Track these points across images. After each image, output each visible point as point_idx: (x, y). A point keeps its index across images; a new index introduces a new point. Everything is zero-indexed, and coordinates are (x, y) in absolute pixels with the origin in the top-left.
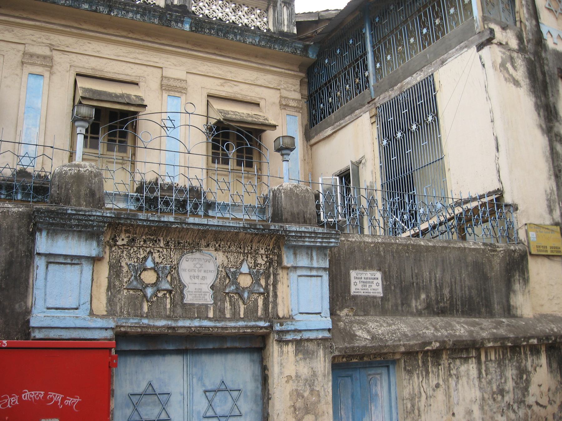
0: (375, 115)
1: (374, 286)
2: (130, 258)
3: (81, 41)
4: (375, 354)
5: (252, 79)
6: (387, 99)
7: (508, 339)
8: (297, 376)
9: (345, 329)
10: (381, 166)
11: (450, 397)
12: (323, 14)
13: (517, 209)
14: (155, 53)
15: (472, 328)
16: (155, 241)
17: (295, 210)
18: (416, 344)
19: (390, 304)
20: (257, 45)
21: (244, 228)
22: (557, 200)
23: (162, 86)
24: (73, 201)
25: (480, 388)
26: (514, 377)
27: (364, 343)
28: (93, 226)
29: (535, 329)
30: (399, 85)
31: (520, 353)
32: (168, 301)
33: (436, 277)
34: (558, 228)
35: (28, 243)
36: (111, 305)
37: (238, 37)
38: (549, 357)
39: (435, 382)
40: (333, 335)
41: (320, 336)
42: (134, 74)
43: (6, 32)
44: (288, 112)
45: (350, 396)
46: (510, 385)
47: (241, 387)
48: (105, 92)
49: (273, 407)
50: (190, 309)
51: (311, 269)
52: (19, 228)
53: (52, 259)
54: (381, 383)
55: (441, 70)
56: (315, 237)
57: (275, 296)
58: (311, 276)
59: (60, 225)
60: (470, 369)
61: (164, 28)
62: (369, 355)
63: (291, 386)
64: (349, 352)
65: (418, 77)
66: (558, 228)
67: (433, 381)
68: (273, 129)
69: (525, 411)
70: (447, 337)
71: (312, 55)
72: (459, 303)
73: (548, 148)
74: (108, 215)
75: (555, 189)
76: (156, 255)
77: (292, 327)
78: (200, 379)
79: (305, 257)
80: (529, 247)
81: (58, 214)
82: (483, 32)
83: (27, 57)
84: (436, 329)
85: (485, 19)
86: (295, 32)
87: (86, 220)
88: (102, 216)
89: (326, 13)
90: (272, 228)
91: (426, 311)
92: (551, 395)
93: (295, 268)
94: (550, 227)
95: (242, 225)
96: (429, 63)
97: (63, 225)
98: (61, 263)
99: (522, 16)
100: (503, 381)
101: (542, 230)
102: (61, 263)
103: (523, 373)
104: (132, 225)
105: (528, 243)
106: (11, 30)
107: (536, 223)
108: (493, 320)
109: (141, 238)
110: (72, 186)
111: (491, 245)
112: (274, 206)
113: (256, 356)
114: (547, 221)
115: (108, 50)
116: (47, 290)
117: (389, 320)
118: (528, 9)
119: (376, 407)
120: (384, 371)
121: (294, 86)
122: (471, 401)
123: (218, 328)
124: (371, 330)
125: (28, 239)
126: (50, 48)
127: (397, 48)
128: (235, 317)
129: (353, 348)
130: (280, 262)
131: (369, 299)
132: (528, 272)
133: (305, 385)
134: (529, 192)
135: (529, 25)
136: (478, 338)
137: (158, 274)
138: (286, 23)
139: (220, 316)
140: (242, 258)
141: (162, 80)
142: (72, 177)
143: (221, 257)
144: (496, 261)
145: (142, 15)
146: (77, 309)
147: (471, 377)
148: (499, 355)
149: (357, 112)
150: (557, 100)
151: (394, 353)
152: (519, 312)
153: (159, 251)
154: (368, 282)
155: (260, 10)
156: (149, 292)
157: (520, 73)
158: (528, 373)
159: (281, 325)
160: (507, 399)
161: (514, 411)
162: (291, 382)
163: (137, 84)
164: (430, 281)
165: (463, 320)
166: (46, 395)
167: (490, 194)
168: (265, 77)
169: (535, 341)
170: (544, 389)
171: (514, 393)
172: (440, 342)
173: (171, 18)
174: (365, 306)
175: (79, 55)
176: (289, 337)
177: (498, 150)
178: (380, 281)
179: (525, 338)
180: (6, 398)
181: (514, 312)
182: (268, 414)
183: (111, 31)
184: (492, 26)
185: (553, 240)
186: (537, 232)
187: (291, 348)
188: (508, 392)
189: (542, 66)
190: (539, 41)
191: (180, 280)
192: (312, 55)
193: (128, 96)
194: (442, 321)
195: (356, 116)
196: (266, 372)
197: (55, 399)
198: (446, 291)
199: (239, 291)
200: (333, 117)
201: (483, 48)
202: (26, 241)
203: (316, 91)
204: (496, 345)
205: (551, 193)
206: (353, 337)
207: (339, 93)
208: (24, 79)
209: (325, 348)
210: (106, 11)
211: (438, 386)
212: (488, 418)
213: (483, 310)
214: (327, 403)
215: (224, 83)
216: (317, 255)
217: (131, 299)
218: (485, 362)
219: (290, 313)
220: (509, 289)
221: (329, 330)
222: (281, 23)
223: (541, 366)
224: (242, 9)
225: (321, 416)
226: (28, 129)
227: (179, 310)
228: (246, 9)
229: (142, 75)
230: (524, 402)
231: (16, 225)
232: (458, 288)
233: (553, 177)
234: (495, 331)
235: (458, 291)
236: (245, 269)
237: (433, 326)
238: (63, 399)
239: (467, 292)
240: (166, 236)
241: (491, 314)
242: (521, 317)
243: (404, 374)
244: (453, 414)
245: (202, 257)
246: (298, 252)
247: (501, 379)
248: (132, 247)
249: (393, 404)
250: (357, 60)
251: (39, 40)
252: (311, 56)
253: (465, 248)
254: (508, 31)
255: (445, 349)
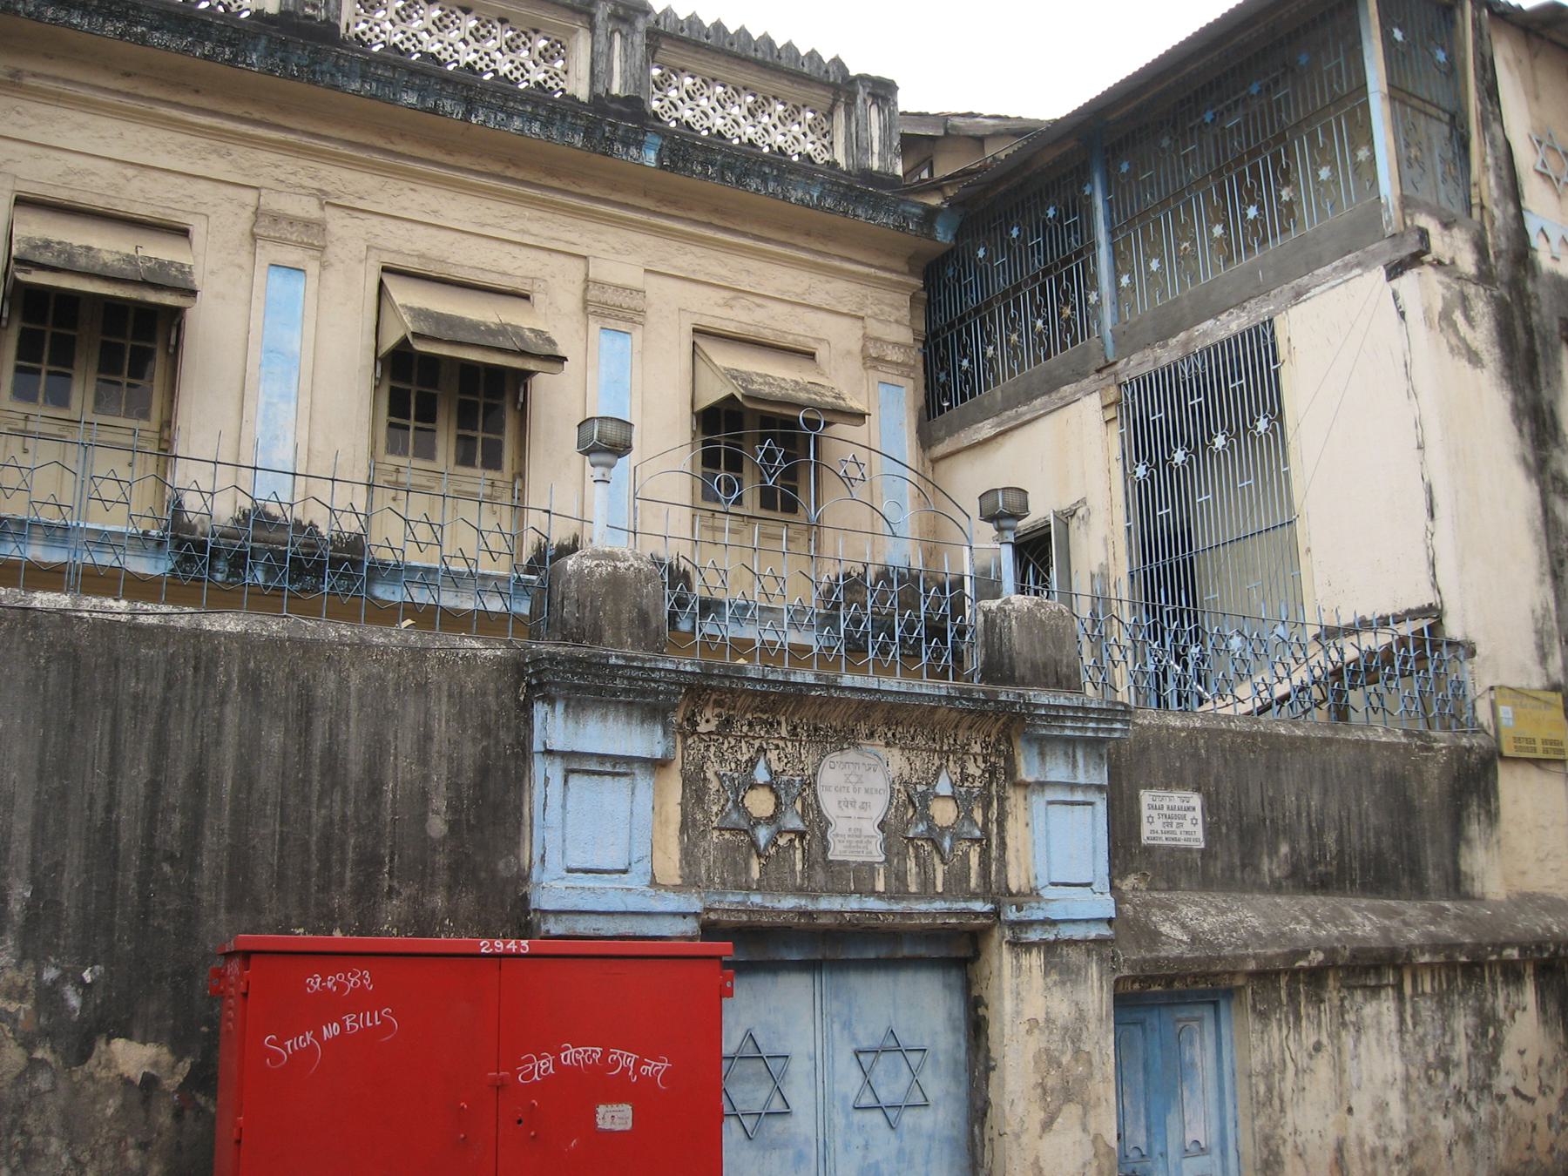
0: (1117, 403)
1: (1187, 826)
2: (722, 761)
3: (394, 185)
4: (1195, 975)
5: (798, 290)
6: (1148, 368)
7: (1460, 946)
8: (1048, 1020)
9: (1136, 920)
10: (1129, 528)
11: (1343, 1071)
12: (957, 121)
13: (1472, 653)
14: (569, 220)
15: (1387, 922)
16: (771, 725)
17: (1040, 657)
18: (1278, 955)
19: (1219, 864)
20: (815, 207)
21: (949, 698)
22: (1556, 632)
23: (586, 303)
24: (608, 634)
25: (1403, 1055)
26: (1470, 1032)
27: (1177, 952)
28: (657, 693)
29: (1512, 926)
30: (1182, 335)
31: (1483, 980)
32: (799, 854)
33: (1309, 806)
34: (1557, 698)
35: (517, 727)
36: (688, 863)
37: (771, 186)
38: (1541, 990)
39: (1313, 1039)
40: (1116, 933)
41: (1093, 935)
42: (518, 273)
43: (214, 157)
44: (883, 377)
45: (1140, 1067)
46: (1461, 1049)
47: (926, 1044)
48: (462, 319)
49: (1002, 1086)
50: (840, 872)
51: (1072, 787)
52: (498, 693)
53: (576, 763)
54: (1202, 1040)
55: (1294, 312)
56: (1083, 719)
57: (1003, 845)
58: (1072, 803)
59: (592, 688)
60: (1382, 1011)
61: (596, 158)
62: (1183, 978)
63: (1035, 1043)
64: (1149, 971)
65: (1234, 323)
66: (1557, 698)
67: (1309, 1036)
68: (856, 421)
69: (1491, 1108)
70: (1338, 939)
71: (944, 236)
72: (1356, 865)
73: (1539, 511)
74: (688, 668)
75: (1552, 606)
76: (773, 755)
77: (1039, 915)
78: (847, 1025)
79: (1061, 762)
80: (1497, 739)
81: (590, 665)
82: (1402, 235)
83: (265, 221)
84: (1315, 923)
85: (1406, 203)
86: (899, 171)
87: (644, 680)
88: (677, 672)
89: (968, 121)
90: (1003, 698)
91: (1290, 882)
92: (1544, 1075)
93: (1042, 785)
94: (1542, 695)
95: (944, 693)
96: (1262, 291)
97: (599, 691)
98: (594, 773)
99: (1485, 195)
100: (1447, 1040)
101: (1525, 701)
102: (594, 773)
103: (1489, 1024)
104: (732, 691)
105: (1497, 731)
106: (224, 151)
107: (1511, 685)
108: (1426, 904)
109: (742, 717)
110: (604, 602)
111: (1420, 735)
112: (987, 644)
113: (954, 977)
114: (1537, 682)
115: (458, 209)
116: (569, 830)
117: (1219, 900)
118: (1499, 177)
119: (1192, 1091)
120: (1207, 1013)
121: (897, 309)
122: (1385, 1082)
123: (895, 914)
124: (1192, 922)
125: (516, 717)
126: (320, 200)
127: (1177, 246)
128: (927, 891)
129: (1157, 960)
130: (1011, 772)
131: (1177, 854)
132: (1497, 799)
133: (1063, 1040)
134: (1496, 614)
135: (1500, 214)
136: (1401, 943)
137: (778, 797)
138: (876, 147)
139: (898, 891)
140: (937, 762)
141: (586, 289)
142: (603, 581)
143: (896, 761)
144: (1433, 771)
145: (544, 125)
146: (625, 872)
147: (1386, 1031)
148: (1440, 984)
149: (1066, 389)
150: (1557, 395)
151: (1233, 974)
152: (1477, 888)
153: (777, 747)
154: (1177, 817)
155: (813, 111)
156: (763, 834)
157: (1482, 335)
158: (1499, 1024)
159: (1019, 909)
160: (1455, 1079)
161: (1469, 1107)
162: (1036, 1031)
163: (527, 297)
164: (1299, 814)
165: (1364, 902)
166: (605, 1054)
167: (1413, 614)
168: (828, 286)
169: (1514, 953)
170: (1531, 1059)
171: (1469, 1067)
172: (1324, 952)
173: (613, 133)
174: (1170, 868)
175: (387, 221)
176: (1033, 936)
177: (1432, 516)
178: (1198, 814)
179: (1494, 945)
180: (530, 1060)
181: (1468, 888)
182: (987, 1102)
183: (464, 161)
184: (1424, 221)
185: (1547, 724)
186: (1514, 706)
187: (1035, 960)
188: (1457, 1065)
189: (1526, 315)
190: (1522, 254)
191: (820, 812)
192: (944, 236)
193: (517, 331)
194: (1324, 904)
195: (1062, 399)
196: (981, 1011)
197: (622, 1063)
198: (1330, 839)
199: (934, 835)
200: (999, 394)
201: (1402, 273)
202: (513, 723)
203: (951, 326)
204: (1436, 960)
205: (1544, 616)
206: (1155, 936)
207: (1014, 337)
208: (259, 278)
209: (1101, 960)
210: (459, 112)
211: (1318, 1047)
212: (1417, 1121)
213: (1405, 882)
214: (1105, 1079)
215: (734, 299)
216: (1085, 757)
217: (727, 849)
218: (1412, 997)
219: (1033, 883)
220: (1458, 836)
221: (1110, 921)
222: (867, 150)
223: (1524, 1009)
224: (771, 110)
225: (1095, 1107)
226: (268, 404)
227: (820, 876)
228: (780, 108)
229: (539, 275)
230: (1489, 1087)
231: (491, 686)
232: (1354, 831)
233: (1548, 579)
234: (1432, 928)
235: (1355, 838)
236: (944, 787)
237: (1309, 916)
238: (638, 1064)
239: (1373, 842)
240: (793, 714)
241: (1419, 891)
242: (1481, 899)
243: (1252, 1022)
244: (1350, 1110)
245: (861, 760)
246: (1047, 749)
247: (1443, 1035)
248: (726, 737)
249: (1227, 1085)
250: (1068, 261)
251: (293, 179)
252: (940, 237)
253: (1368, 743)
254: (1456, 231)
255: (1335, 967)
